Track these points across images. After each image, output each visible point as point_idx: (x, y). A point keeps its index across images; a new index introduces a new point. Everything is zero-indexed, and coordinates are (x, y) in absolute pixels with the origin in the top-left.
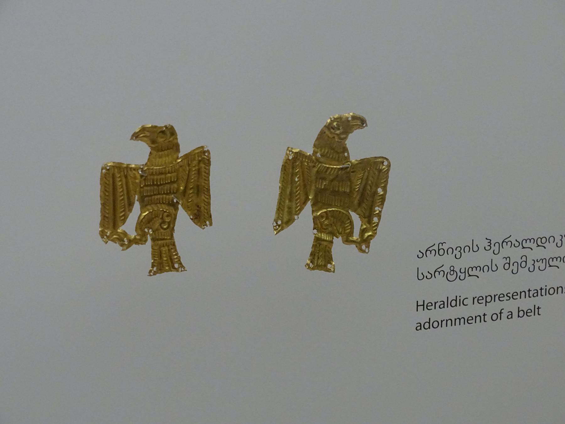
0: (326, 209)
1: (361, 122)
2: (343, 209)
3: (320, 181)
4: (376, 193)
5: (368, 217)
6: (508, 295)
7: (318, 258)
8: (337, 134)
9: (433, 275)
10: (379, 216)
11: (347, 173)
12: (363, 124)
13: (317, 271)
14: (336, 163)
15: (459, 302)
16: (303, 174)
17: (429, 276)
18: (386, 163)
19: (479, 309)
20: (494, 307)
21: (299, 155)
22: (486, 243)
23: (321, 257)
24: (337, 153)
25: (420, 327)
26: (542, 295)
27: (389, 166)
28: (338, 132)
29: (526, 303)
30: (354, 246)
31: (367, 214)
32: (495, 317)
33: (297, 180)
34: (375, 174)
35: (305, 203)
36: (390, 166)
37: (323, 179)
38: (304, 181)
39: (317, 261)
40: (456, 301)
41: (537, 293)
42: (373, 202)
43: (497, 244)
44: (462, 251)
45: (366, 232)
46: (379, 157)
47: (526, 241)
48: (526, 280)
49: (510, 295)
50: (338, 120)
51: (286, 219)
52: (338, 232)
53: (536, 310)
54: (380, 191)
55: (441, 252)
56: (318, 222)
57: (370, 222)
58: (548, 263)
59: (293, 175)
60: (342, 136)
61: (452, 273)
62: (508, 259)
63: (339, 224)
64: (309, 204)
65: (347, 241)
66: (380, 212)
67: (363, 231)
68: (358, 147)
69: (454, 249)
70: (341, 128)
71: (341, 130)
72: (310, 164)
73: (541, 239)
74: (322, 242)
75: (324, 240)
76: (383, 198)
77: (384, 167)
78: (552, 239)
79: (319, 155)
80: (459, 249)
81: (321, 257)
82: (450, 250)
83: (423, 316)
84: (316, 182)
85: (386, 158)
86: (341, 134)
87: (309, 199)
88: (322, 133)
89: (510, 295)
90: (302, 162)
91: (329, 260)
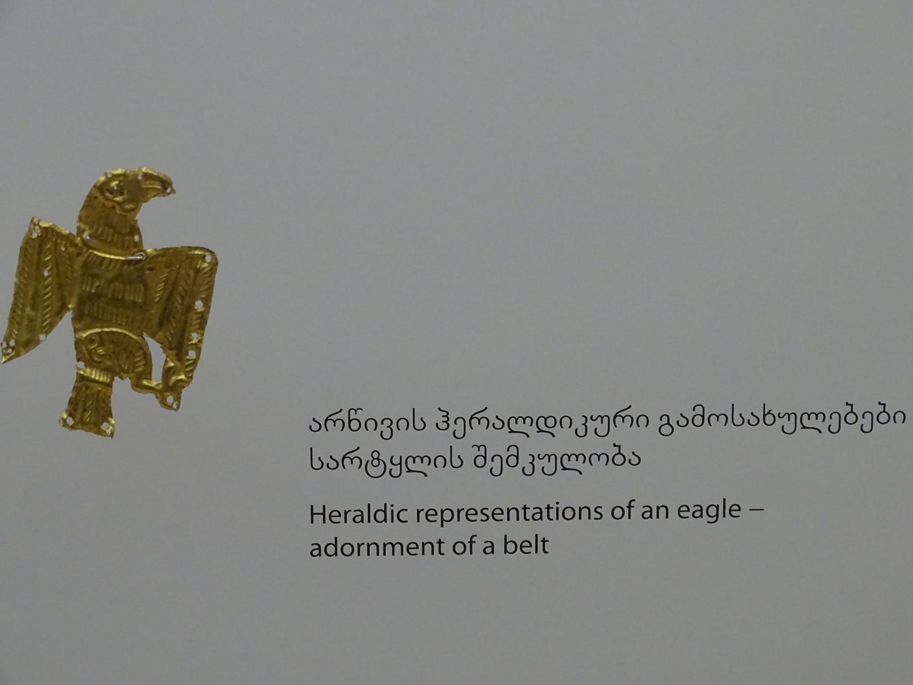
0: (102, 327)
1: (165, 186)
2: (130, 331)
3: (90, 279)
4: (190, 308)
5: (178, 347)
6: (484, 511)
7: (85, 410)
8: (119, 203)
9: (340, 464)
10: (197, 348)
11: (139, 271)
12: (166, 189)
13: (80, 433)
14: (119, 252)
15: (389, 514)
16: (57, 265)
18: (208, 258)
19: (430, 531)
20: (459, 530)
21: (49, 234)
22: (440, 419)
23: (88, 409)
24: (120, 233)
25: (318, 550)
26: (549, 519)
27: (214, 265)
28: (119, 199)
29: (521, 531)
30: (151, 396)
31: (174, 344)
32: (459, 548)
33: (46, 274)
34: (189, 275)
35: (59, 313)
36: (217, 264)
37: (95, 276)
38: (58, 276)
39: (83, 415)
40: (385, 512)
41: (541, 513)
42: (185, 322)
43: (460, 421)
44: (394, 427)
45: (174, 373)
46: (197, 248)
48: (512, 489)
49: (489, 513)
50: (121, 178)
51: (25, 337)
52: (122, 369)
53: (540, 544)
54: (199, 305)
55: (355, 425)
56: (84, 348)
57: (180, 357)
58: (561, 462)
59: (40, 265)
60: (128, 206)
61: (376, 462)
62: (482, 448)
63: (124, 356)
64: (68, 316)
65: (138, 386)
66: (200, 341)
67: (168, 372)
68: (159, 227)
70: (125, 192)
71: (125, 196)
72: (71, 250)
73: (546, 419)
74: (92, 384)
75: (94, 381)
76: (203, 319)
77: (206, 265)
78: (566, 422)
79: (86, 236)
80: (387, 422)
81: (88, 409)
82: (371, 424)
83: (324, 533)
84: (82, 282)
85: (208, 251)
86: (125, 201)
87: (68, 309)
88: (91, 199)
89: (489, 513)
90: (56, 245)
91: (105, 414)
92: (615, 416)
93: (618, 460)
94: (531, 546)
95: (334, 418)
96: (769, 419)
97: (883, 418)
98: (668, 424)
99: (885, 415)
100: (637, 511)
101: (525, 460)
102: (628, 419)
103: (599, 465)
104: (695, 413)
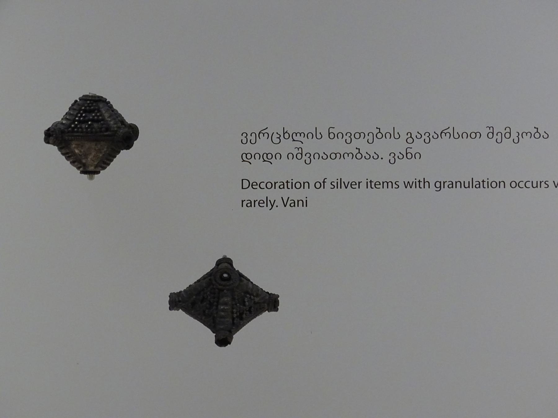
17: (325, 157)
41: (479, 184)
44: (520, 136)
47: (296, 134)
69: (344, 135)
92: (260, 133)
93: (359, 156)
94: (264, 203)
95: (445, 131)
96: (287, 136)
97: (379, 135)
98: (411, 137)
99: (537, 134)
100: (328, 185)
101: (514, 135)
102: (266, 135)
103: (348, 159)
104: (506, 131)
